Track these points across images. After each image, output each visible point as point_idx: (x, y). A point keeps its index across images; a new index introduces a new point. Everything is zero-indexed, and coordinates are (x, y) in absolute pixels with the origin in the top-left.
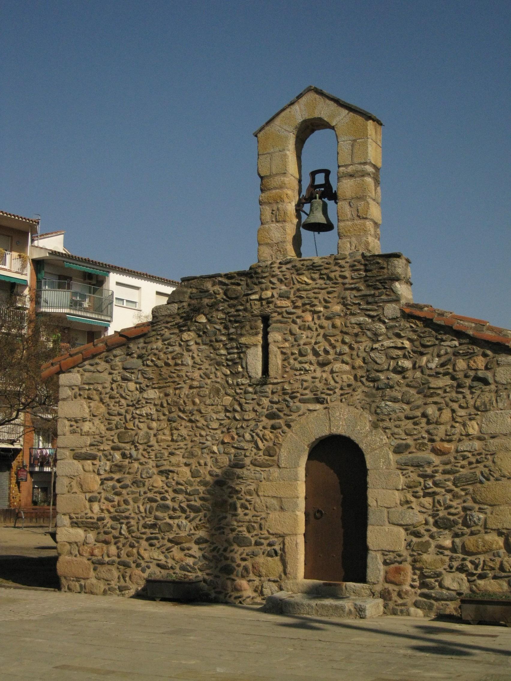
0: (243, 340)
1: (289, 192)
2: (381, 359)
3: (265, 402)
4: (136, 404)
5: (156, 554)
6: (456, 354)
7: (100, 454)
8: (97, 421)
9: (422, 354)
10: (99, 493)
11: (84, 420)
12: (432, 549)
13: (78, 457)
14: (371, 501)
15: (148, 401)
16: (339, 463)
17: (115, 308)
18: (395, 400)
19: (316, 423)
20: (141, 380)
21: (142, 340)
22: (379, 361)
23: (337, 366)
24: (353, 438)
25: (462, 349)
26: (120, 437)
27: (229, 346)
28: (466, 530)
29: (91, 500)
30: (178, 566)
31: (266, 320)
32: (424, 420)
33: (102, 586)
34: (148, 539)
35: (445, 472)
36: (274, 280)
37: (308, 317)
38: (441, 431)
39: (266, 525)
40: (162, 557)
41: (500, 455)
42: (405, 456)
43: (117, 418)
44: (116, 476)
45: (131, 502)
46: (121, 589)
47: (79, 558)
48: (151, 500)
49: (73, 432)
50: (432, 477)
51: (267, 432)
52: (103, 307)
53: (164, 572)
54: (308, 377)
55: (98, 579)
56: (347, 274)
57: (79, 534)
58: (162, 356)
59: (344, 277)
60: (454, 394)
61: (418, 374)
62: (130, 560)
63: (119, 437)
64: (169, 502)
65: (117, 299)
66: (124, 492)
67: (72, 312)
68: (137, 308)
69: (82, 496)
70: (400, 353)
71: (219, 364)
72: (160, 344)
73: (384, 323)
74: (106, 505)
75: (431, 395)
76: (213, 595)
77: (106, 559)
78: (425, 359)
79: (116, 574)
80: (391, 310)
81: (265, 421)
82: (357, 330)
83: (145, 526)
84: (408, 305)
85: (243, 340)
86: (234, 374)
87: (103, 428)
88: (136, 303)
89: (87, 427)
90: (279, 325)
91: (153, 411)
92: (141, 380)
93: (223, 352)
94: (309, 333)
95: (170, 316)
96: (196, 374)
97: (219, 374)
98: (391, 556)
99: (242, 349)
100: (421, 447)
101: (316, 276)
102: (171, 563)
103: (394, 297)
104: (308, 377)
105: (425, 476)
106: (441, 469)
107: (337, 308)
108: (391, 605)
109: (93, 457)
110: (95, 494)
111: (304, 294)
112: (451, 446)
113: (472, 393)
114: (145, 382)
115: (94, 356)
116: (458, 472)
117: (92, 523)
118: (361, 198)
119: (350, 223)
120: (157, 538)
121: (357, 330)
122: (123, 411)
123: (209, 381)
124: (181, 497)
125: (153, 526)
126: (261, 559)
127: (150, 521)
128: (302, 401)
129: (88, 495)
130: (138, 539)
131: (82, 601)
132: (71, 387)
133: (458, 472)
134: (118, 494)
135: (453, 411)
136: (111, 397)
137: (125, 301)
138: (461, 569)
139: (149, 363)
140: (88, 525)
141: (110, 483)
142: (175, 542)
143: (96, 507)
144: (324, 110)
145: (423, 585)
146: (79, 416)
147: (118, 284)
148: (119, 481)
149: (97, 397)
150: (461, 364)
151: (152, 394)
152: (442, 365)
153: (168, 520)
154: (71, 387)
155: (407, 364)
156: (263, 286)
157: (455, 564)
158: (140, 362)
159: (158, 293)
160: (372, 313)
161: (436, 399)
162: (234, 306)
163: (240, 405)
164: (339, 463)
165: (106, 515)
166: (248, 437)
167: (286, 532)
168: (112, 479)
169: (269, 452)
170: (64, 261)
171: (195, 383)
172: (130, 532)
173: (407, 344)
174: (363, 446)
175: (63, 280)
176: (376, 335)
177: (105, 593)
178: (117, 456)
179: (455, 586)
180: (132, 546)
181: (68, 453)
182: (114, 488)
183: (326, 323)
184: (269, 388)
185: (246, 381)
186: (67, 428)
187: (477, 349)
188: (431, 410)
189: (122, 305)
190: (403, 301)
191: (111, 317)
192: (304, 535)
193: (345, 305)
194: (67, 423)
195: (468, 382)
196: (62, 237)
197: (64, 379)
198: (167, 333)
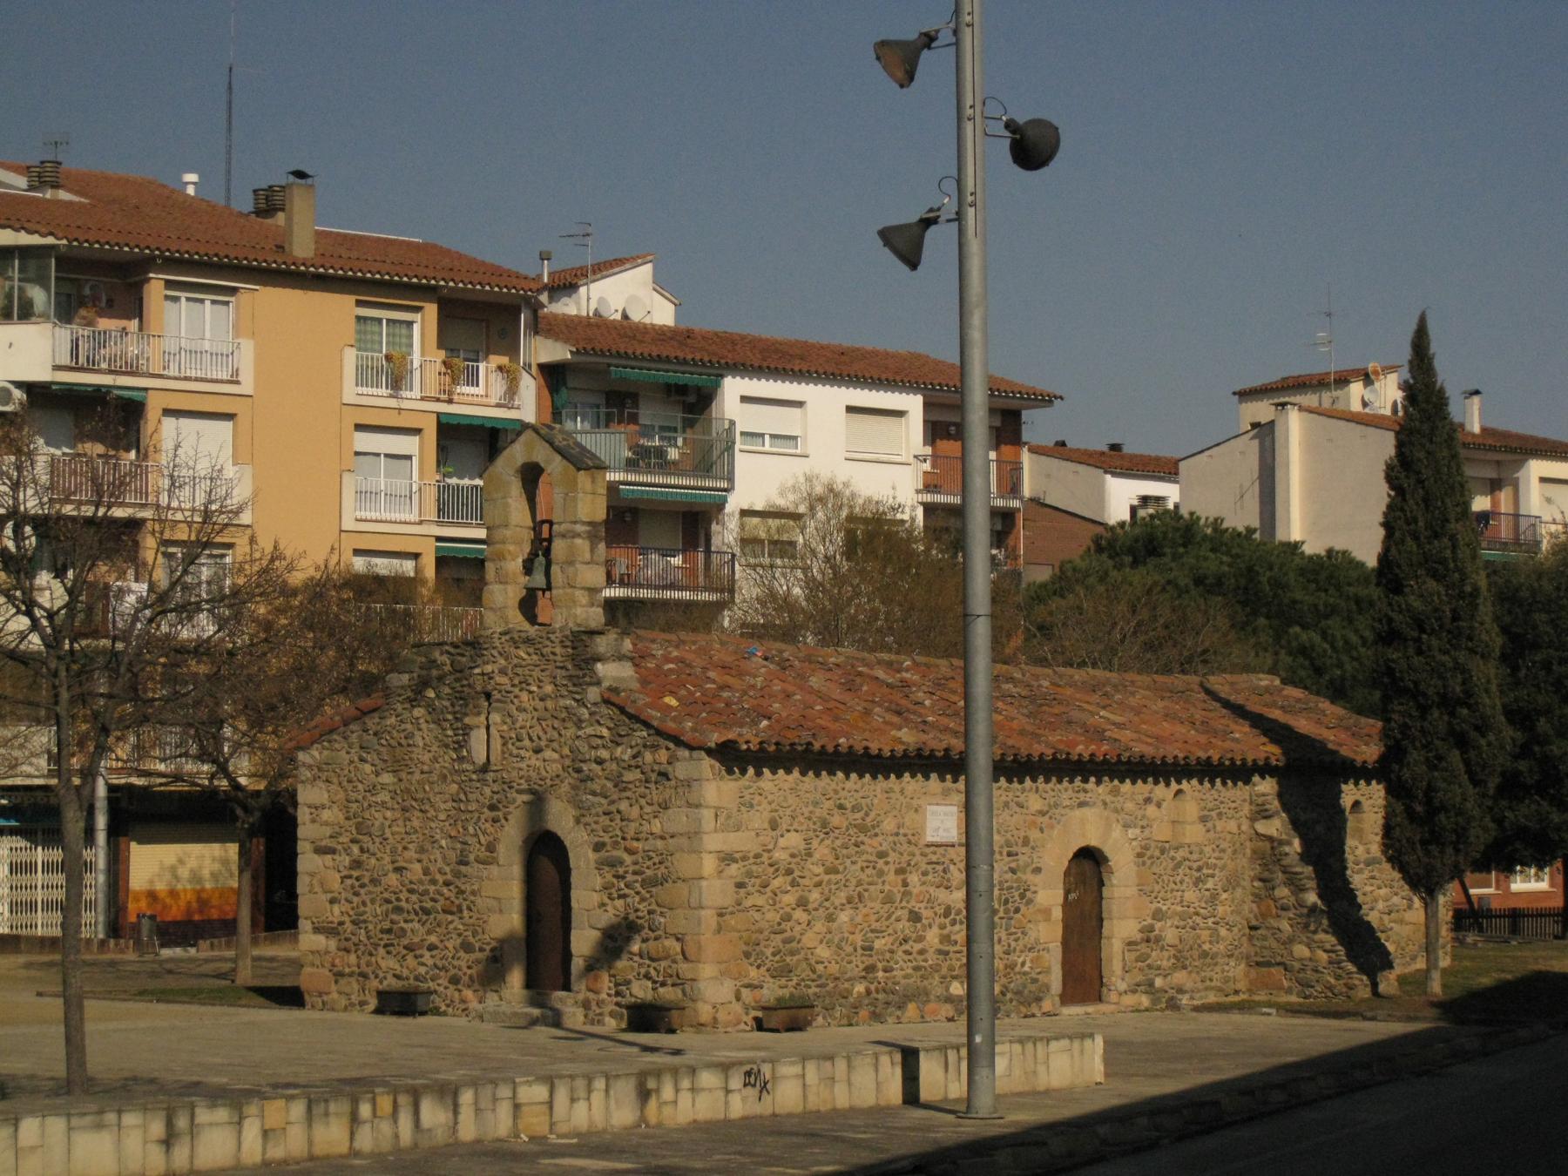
0: (467, 720)
1: (511, 548)
2: (584, 748)
3: (487, 791)
4: (372, 790)
7: (339, 847)
8: (336, 810)
9: (618, 744)
15: (383, 786)
17: (739, 458)
18: (594, 794)
20: (377, 762)
21: (376, 715)
23: (548, 754)
25: (650, 741)
26: (358, 827)
28: (652, 935)
31: (488, 696)
32: (618, 817)
33: (344, 1002)
34: (386, 946)
35: (635, 873)
36: (495, 653)
37: (524, 696)
38: (631, 829)
39: (487, 928)
40: (397, 966)
41: (677, 855)
42: (603, 854)
43: (354, 806)
44: (355, 874)
46: (362, 1003)
47: (321, 970)
48: (388, 901)
49: (313, 821)
50: (623, 877)
51: (488, 825)
52: (713, 459)
53: (400, 983)
54: (523, 765)
55: (340, 993)
56: (558, 650)
57: (320, 941)
58: (395, 734)
59: (554, 654)
60: (643, 789)
61: (614, 766)
62: (369, 970)
64: (403, 904)
65: (742, 434)
66: (362, 891)
67: (631, 477)
68: (798, 451)
70: (599, 742)
72: (393, 720)
74: (346, 907)
75: (624, 789)
76: (443, 1008)
77: (347, 970)
78: (619, 750)
79: (356, 986)
80: (593, 694)
81: (487, 813)
82: (564, 715)
83: (382, 931)
85: (467, 720)
86: (461, 759)
87: (341, 816)
88: (795, 438)
89: (326, 815)
91: (387, 799)
92: (377, 762)
99: (467, 730)
101: (531, 650)
102: (405, 973)
104: (523, 765)
105: (617, 877)
106: (631, 869)
107: (549, 688)
108: (591, 1015)
109: (333, 851)
111: (520, 671)
112: (639, 845)
114: (381, 765)
115: (331, 731)
118: (571, 563)
121: (564, 715)
124: (414, 898)
125: (389, 931)
127: (387, 925)
128: (519, 792)
129: (329, 896)
130: (376, 946)
131: (316, 1015)
132: (310, 767)
134: (356, 894)
136: (350, 781)
138: (647, 976)
140: (329, 931)
141: (349, 882)
143: (336, 909)
145: (618, 994)
146: (318, 802)
147: (745, 399)
148: (357, 879)
149: (335, 780)
150: (648, 757)
151: (387, 778)
152: (634, 757)
154: (310, 767)
155: (604, 754)
157: (643, 971)
158: (375, 740)
159: (851, 409)
161: (628, 794)
165: (347, 919)
166: (471, 830)
168: (350, 877)
169: (491, 848)
170: (609, 365)
171: (426, 768)
172: (369, 938)
173: (605, 732)
174: (567, 843)
175: (618, 403)
176: (581, 721)
177: (346, 1009)
178: (355, 849)
179: (641, 994)
180: (371, 954)
182: (353, 887)
183: (540, 705)
184: (490, 776)
185: (471, 768)
186: (308, 817)
187: (662, 742)
188: (623, 806)
189: (760, 449)
190: (606, 684)
191: (731, 479)
194: (307, 810)
195: (654, 776)
196: (649, 266)
197: (302, 756)
198: (399, 707)
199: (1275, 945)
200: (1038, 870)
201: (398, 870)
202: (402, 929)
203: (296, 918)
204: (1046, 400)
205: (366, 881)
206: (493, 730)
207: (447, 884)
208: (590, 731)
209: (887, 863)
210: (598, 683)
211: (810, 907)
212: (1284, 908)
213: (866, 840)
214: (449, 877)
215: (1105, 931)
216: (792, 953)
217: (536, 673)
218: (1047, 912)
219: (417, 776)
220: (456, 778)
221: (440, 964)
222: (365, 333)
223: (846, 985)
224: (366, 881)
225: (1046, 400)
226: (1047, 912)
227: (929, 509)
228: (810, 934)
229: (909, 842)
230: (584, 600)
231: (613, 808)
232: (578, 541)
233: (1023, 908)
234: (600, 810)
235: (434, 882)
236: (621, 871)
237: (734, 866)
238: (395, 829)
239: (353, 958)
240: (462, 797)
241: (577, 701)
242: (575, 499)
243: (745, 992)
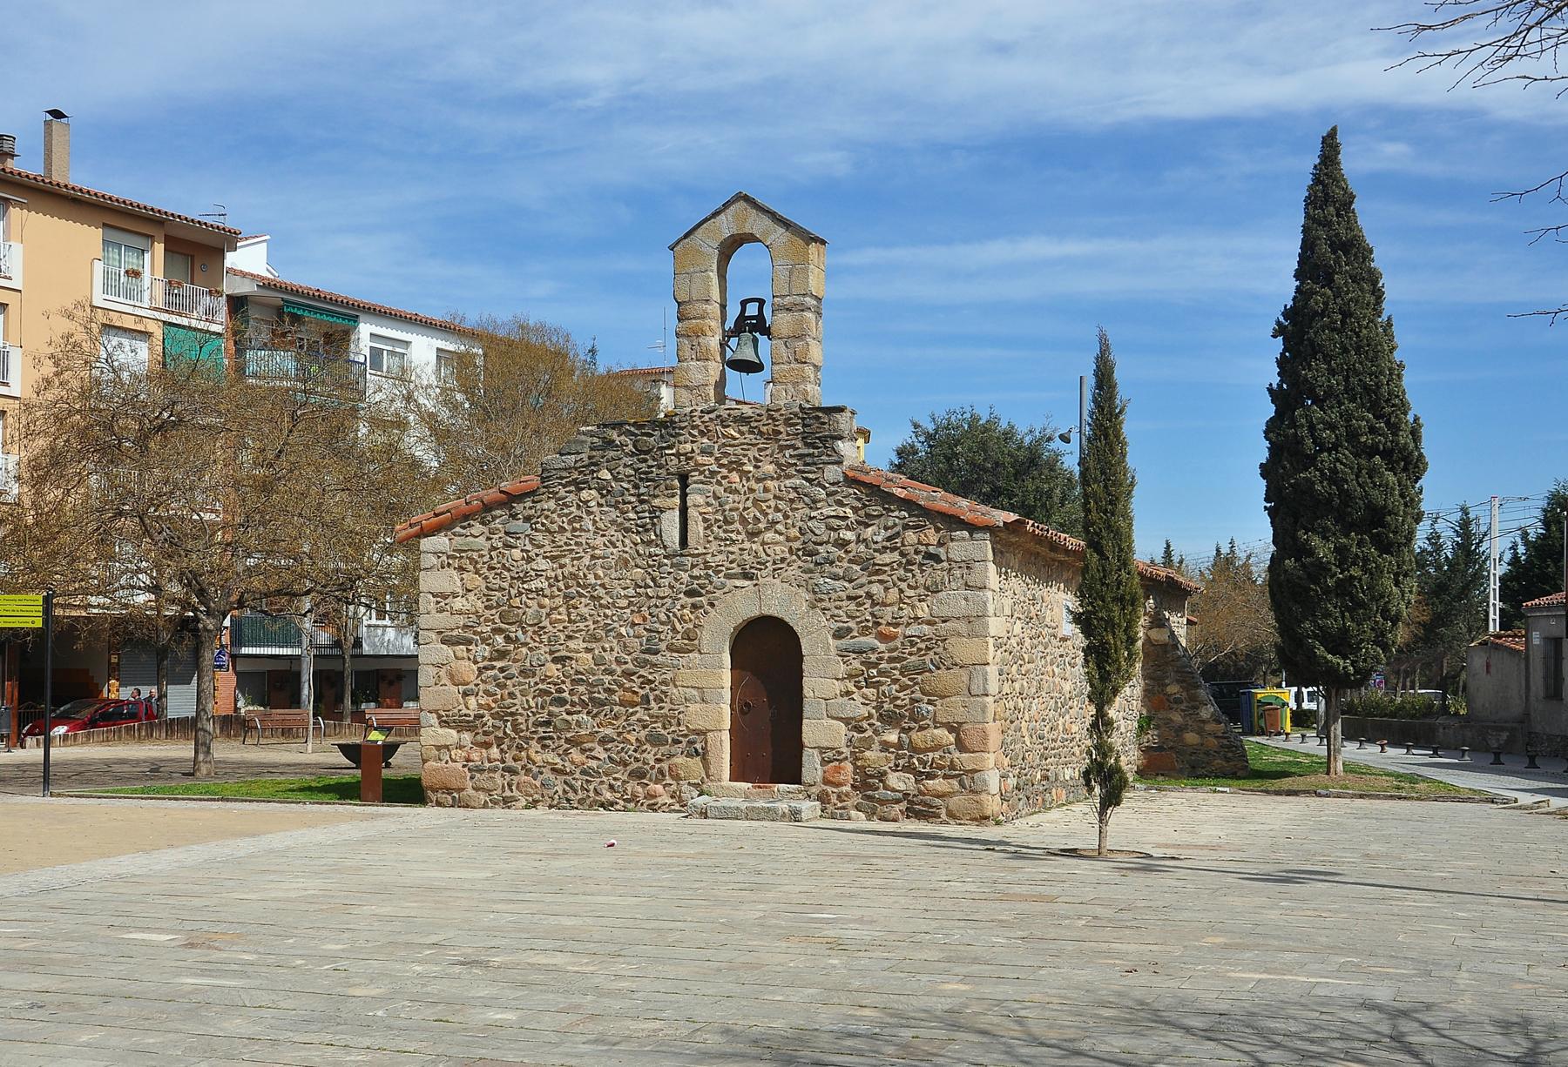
2: (820, 528)
3: (685, 577)
18: (836, 577)
37: (735, 476)
73: (824, 488)
85: (656, 502)
94: (736, 498)
99: (656, 513)
111: (730, 450)
155: (850, 535)
162: (645, 461)
210: (839, 463)
234: (843, 595)
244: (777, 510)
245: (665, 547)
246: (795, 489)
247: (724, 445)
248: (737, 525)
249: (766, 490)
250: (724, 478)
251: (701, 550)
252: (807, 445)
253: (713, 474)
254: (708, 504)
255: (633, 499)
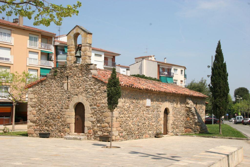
5: (47, 128)
6: (101, 86)
10: (36, 115)
11: (33, 99)
12: (96, 127)
13: (32, 107)
14: (85, 116)
16: (79, 108)
18: (90, 95)
19: (76, 100)
22: (87, 87)
24: (83, 103)
26: (40, 103)
27: (61, 83)
29: (34, 116)
30: (51, 131)
34: (45, 124)
40: (47, 128)
42: (92, 107)
45: (131, 112)
47: (32, 129)
48: (46, 116)
49: (31, 101)
63: (40, 103)
64: (49, 117)
69: (33, 115)
71: (59, 87)
73: (89, 79)
77: (37, 129)
80: (90, 76)
84: (93, 75)
85: (63, 81)
89: (33, 100)
90: (70, 79)
92: (44, 90)
93: (60, 84)
94: (75, 81)
95: (50, 76)
96: (54, 89)
97: (59, 89)
98: (89, 128)
99: (63, 83)
100: (95, 105)
103: (90, 73)
106: (98, 110)
107: (80, 75)
109: (35, 107)
110: (35, 115)
111: (74, 72)
113: (104, 94)
116: (101, 110)
117: (34, 121)
119: (83, 57)
120: (47, 124)
122: (41, 97)
123: (57, 91)
125: (46, 122)
126: (66, 129)
129: (34, 115)
130: (43, 125)
133: (101, 110)
135: (100, 98)
137: (7, 34)
138: (101, 131)
139: (46, 86)
142: (50, 125)
144: (79, 31)
146: (32, 97)
153: (49, 120)
155: (92, 87)
156: (67, 70)
157: (100, 130)
160: (86, 76)
162: (62, 74)
163: (63, 96)
164: (79, 108)
167: (70, 123)
168: (38, 112)
169: (68, 106)
174: (84, 105)
181: (30, 106)
188: (96, 97)
192: (75, 123)
193: (82, 75)
199: (189, 125)
200: (160, 112)
201: (48, 110)
202: (49, 121)
203: (27, 119)
204: (119, 55)
205: (42, 112)
206: (69, 83)
207: (59, 113)
208: (89, 83)
209: (141, 109)
210: (91, 74)
211: (130, 117)
212: (191, 119)
213: (138, 105)
214: (59, 112)
215: (168, 122)
216: (127, 126)
217: (78, 73)
218: (161, 119)
219: (53, 92)
220: (61, 92)
221: (56, 128)
222: (30, 38)
223: (135, 132)
224: (42, 112)
225: (119, 55)
226: (161, 119)
227: (104, 67)
228: (130, 122)
229: (144, 106)
230: (88, 58)
231: (94, 98)
232: (87, 47)
233: (159, 118)
234: (91, 98)
235: (56, 113)
236: (96, 110)
237: (119, 109)
238: (48, 102)
239: (38, 127)
240: (62, 96)
241: (87, 77)
242: (87, 39)
243: (120, 134)
244: (82, 83)
245: (64, 90)
246: (84, 79)
247: (74, 71)
248: (76, 86)
249: (80, 79)
250: (74, 77)
251: (70, 90)
252: (87, 71)
253: (72, 76)
254: (71, 82)
255: (60, 81)
